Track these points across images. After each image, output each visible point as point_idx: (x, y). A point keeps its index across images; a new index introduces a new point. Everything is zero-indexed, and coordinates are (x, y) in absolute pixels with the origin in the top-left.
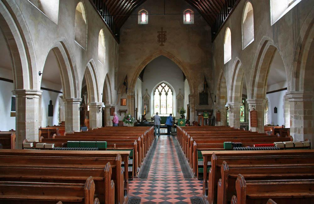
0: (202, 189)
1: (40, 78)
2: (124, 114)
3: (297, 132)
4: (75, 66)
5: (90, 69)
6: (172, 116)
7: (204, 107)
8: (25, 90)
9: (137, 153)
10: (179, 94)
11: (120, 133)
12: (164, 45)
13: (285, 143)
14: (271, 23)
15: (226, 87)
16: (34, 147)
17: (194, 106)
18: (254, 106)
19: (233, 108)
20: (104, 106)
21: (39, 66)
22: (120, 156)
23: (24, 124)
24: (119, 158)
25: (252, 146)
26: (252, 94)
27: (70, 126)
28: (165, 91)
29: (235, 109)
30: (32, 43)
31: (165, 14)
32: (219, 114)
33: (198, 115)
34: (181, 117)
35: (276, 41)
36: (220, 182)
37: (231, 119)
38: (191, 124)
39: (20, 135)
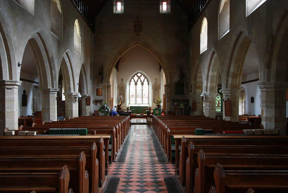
0: (174, 171)
2: (100, 104)
3: (268, 120)
4: (52, 57)
5: (67, 59)
8: (5, 80)
9: (116, 139)
10: (155, 84)
11: (98, 122)
12: (140, 35)
13: (253, 130)
14: (246, 14)
15: (201, 77)
17: (170, 96)
18: (229, 96)
19: (208, 98)
20: (80, 96)
22: (103, 139)
24: (102, 141)
26: (227, 84)
27: (47, 116)
28: (141, 81)
29: (210, 99)
30: (11, 35)
31: (141, 5)
32: (195, 104)
33: (173, 104)
34: (157, 107)
36: (197, 172)
37: (206, 109)
38: (166, 114)
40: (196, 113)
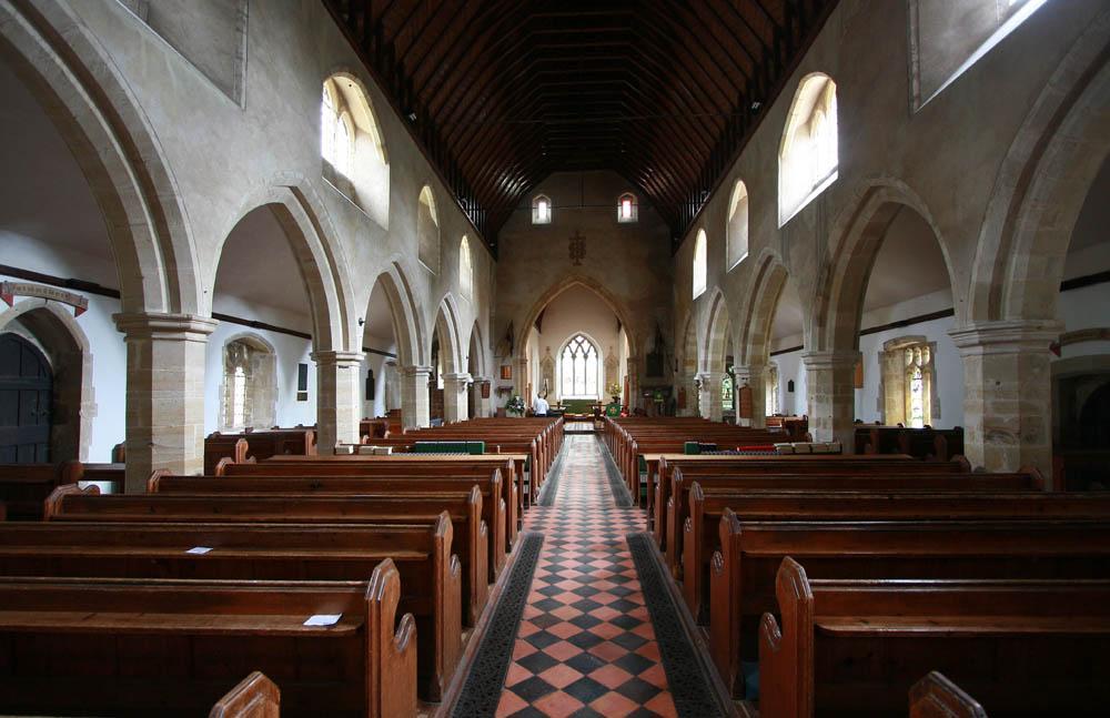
1: (361, 330)
4: (421, 307)
5: (447, 312)
6: (930, 455)
7: (654, 381)
13: (793, 444)
15: (696, 344)
16: (356, 452)
20: (471, 380)
21: (359, 309)
23: (334, 413)
24: (511, 466)
25: (734, 449)
26: (744, 356)
32: (683, 394)
35: (786, 258)
37: (704, 404)
39: (326, 434)
40: (686, 413)
